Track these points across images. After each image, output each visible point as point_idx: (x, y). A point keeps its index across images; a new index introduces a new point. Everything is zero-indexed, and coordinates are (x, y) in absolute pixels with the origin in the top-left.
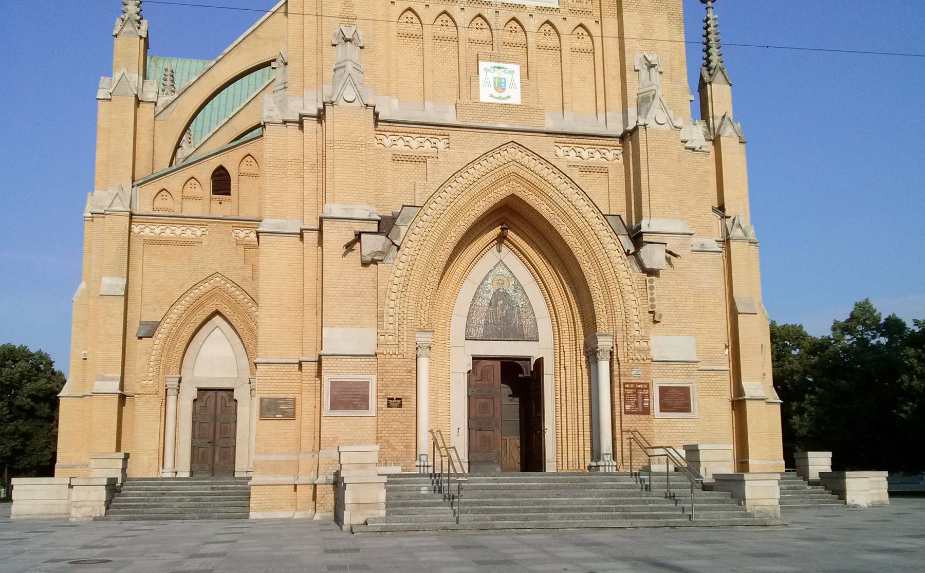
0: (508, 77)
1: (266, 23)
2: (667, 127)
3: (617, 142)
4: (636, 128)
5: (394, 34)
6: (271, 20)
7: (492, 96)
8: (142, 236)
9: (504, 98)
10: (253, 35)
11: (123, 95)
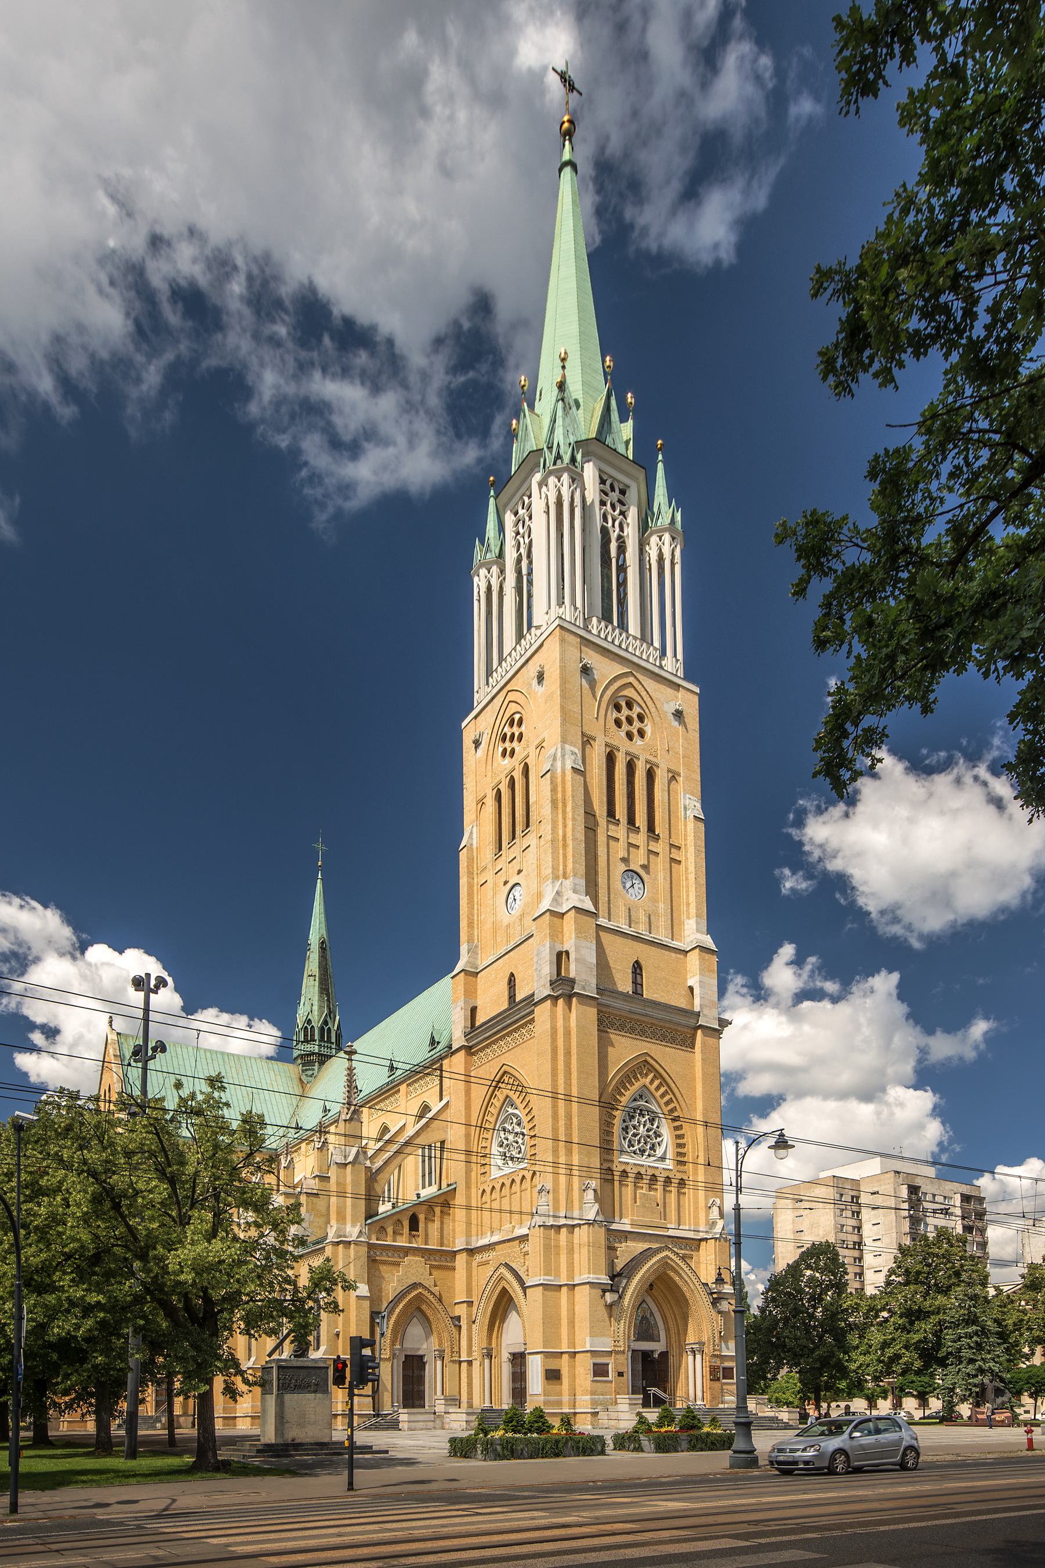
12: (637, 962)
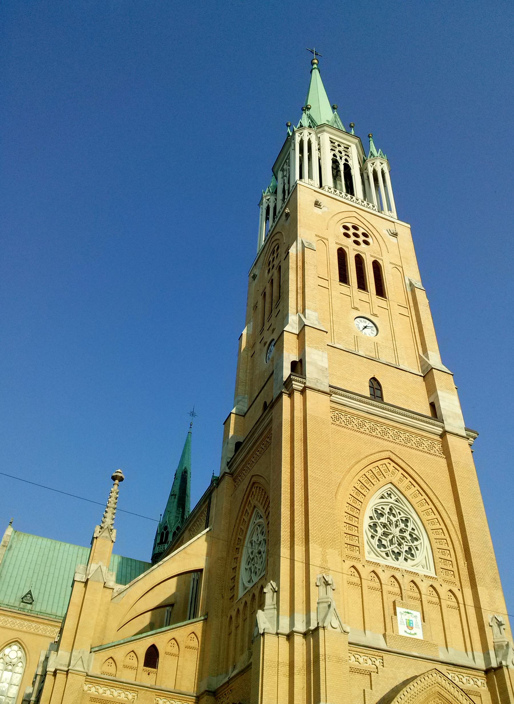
0: (414, 620)
1: (193, 544)
2: (339, 630)
3: (482, 674)
4: (317, 629)
5: (345, 582)
6: (196, 543)
7: (405, 632)
8: (89, 694)
9: (413, 634)
10: (183, 551)
11: (97, 581)
12: (374, 379)
